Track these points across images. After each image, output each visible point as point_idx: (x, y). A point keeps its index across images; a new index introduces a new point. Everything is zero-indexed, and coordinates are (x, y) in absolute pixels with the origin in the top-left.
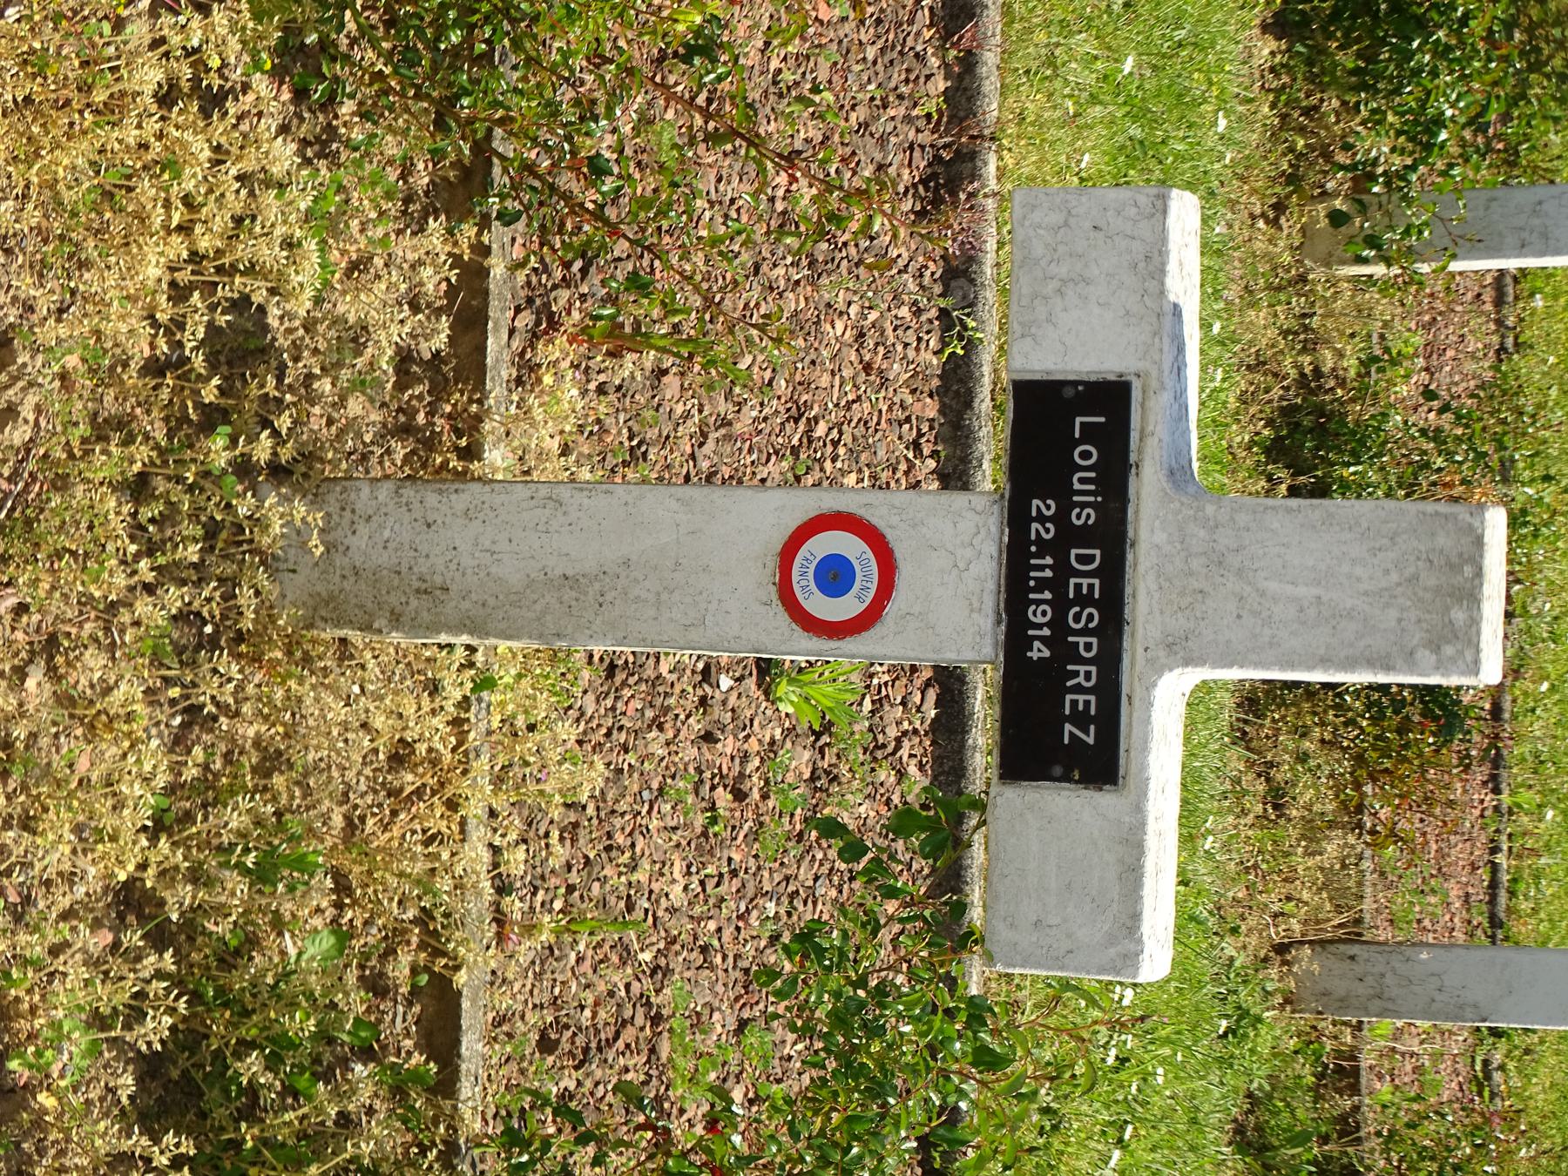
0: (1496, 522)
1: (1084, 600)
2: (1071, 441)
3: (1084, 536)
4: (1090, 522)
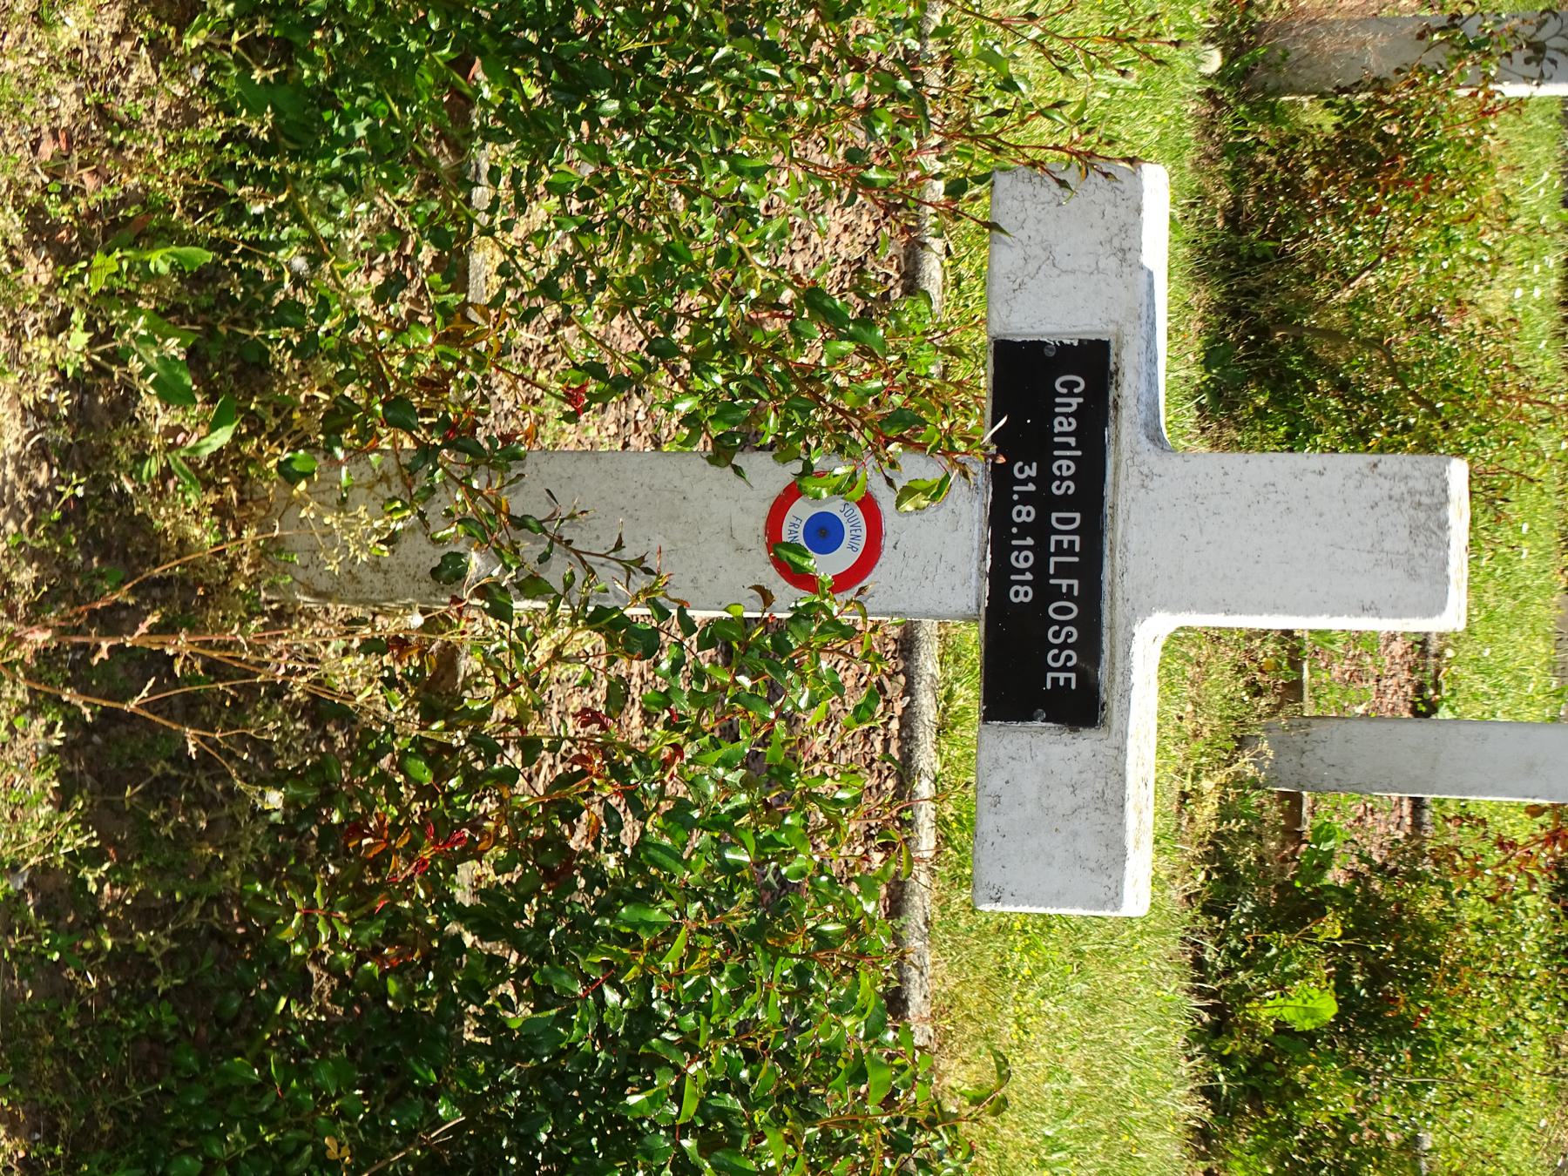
0: (1458, 472)
1: (1026, 499)
2: (1050, 398)
3: (1065, 503)
4: (1070, 492)
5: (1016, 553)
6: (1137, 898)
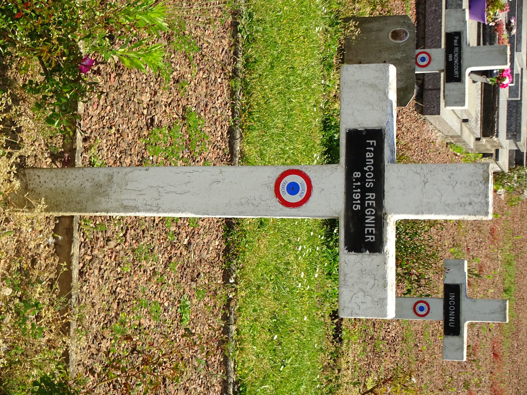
5: (355, 205)
6: (391, 313)
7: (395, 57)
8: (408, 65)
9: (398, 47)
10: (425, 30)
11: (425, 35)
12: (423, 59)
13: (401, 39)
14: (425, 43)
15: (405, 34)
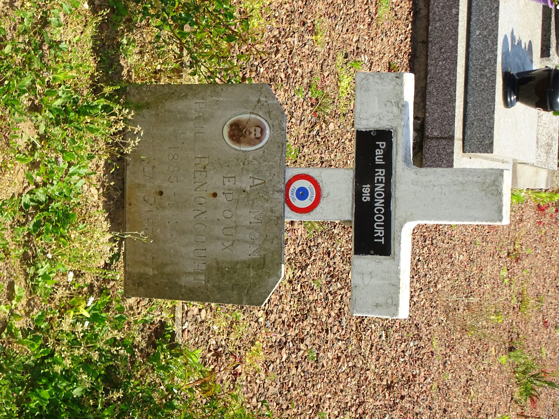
7: (238, 184)
8: (267, 205)
9: (243, 162)
10: (428, 29)
11: (428, 38)
12: (302, 194)
13: (251, 143)
14: (427, 51)
15: (259, 130)
